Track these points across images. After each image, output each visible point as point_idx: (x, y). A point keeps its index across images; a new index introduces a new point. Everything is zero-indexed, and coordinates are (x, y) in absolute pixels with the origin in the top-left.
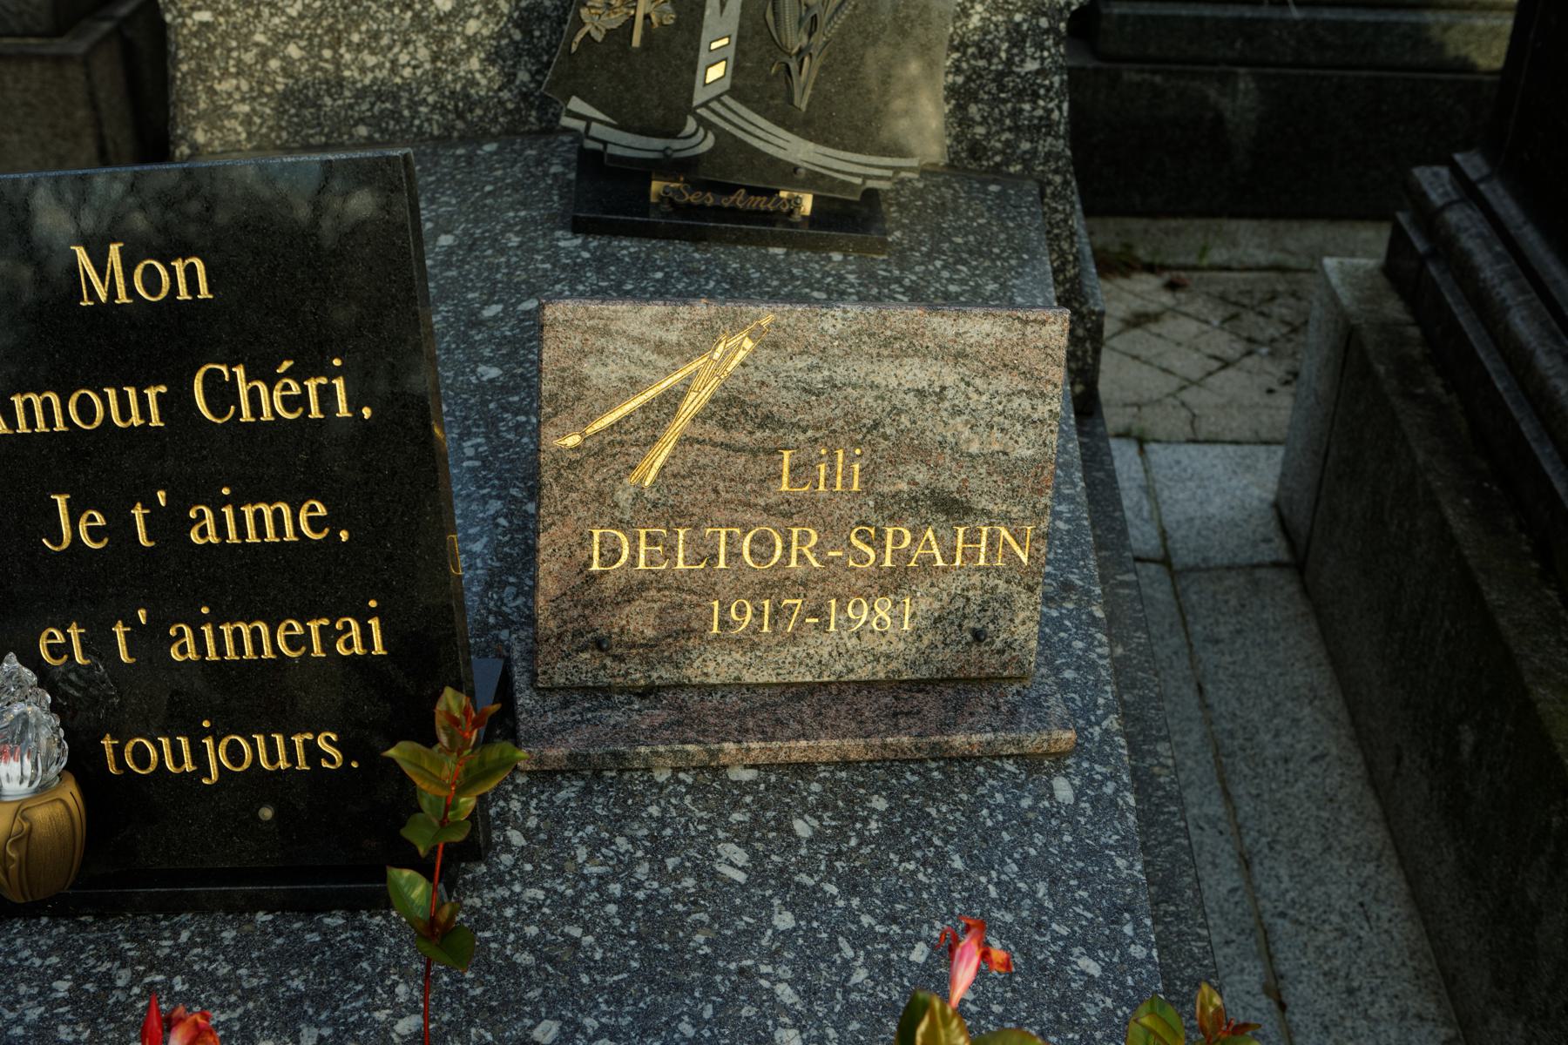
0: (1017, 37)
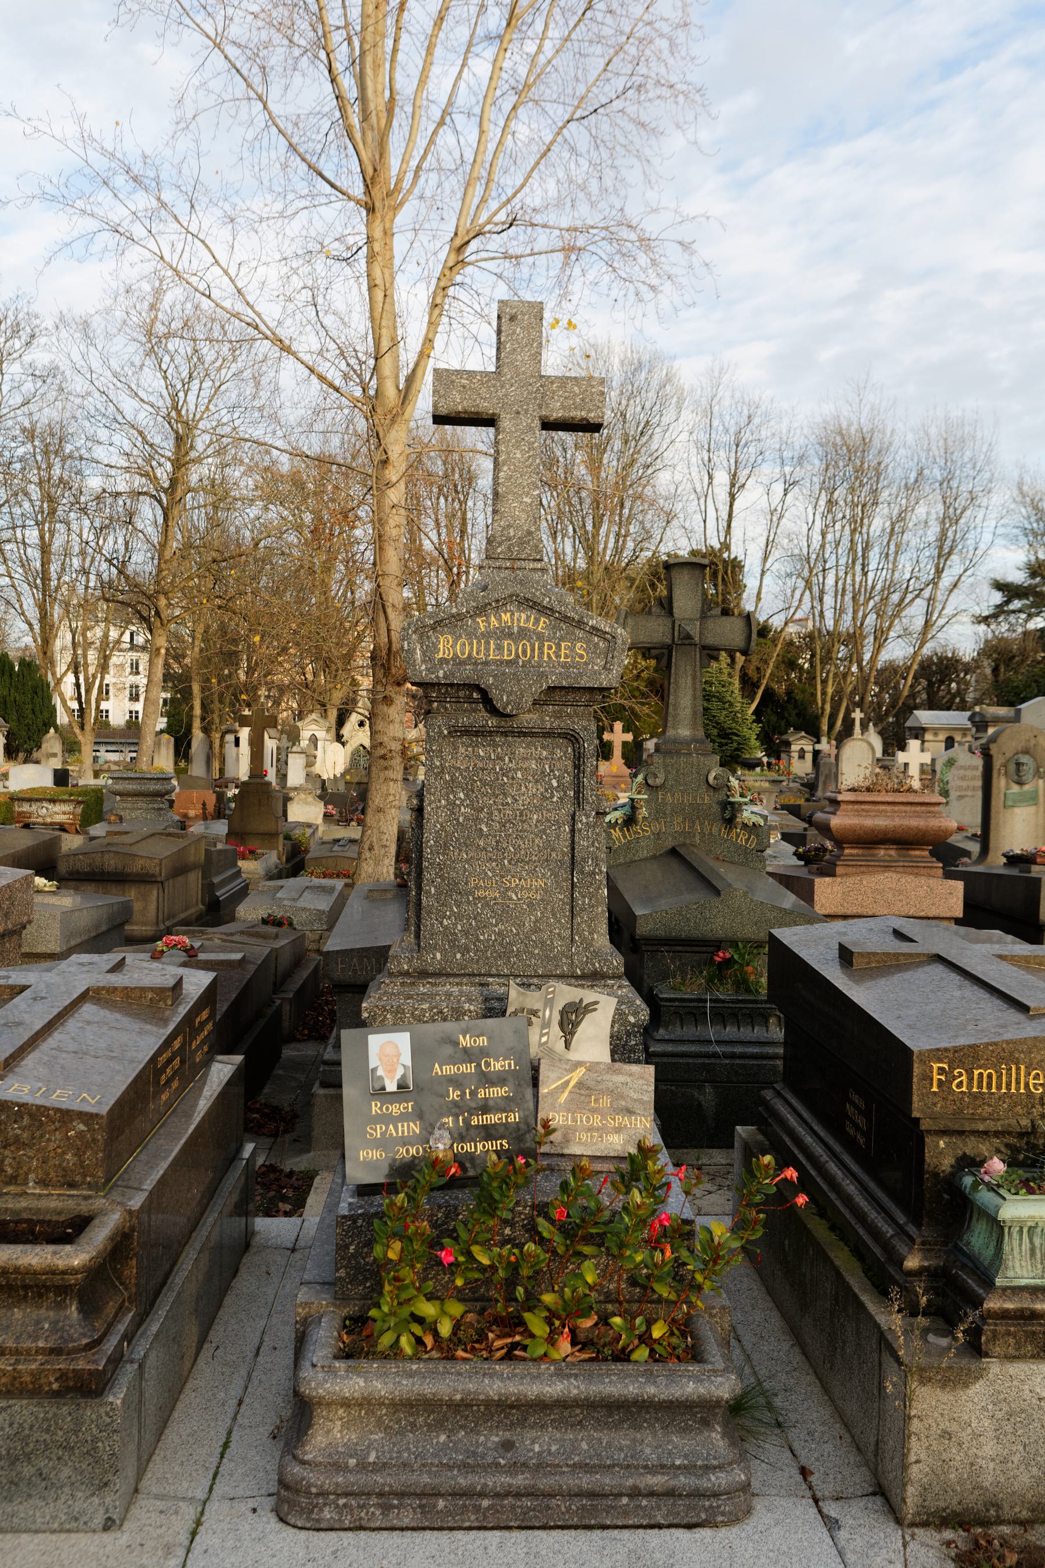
0: (628, 1034)
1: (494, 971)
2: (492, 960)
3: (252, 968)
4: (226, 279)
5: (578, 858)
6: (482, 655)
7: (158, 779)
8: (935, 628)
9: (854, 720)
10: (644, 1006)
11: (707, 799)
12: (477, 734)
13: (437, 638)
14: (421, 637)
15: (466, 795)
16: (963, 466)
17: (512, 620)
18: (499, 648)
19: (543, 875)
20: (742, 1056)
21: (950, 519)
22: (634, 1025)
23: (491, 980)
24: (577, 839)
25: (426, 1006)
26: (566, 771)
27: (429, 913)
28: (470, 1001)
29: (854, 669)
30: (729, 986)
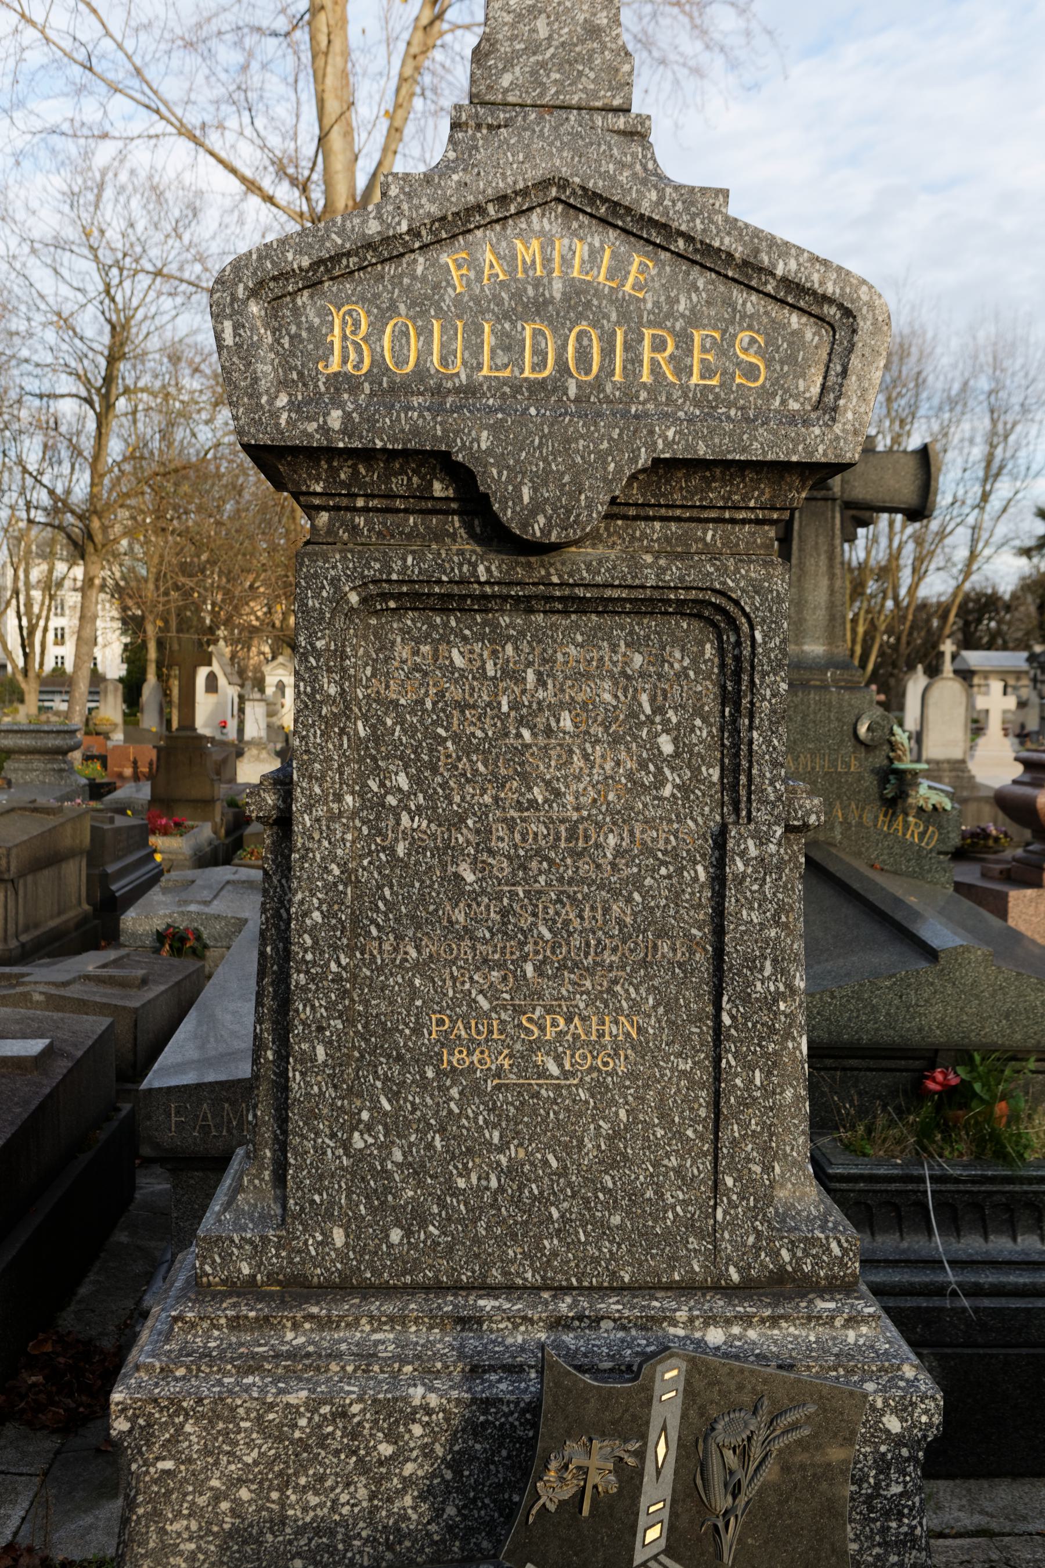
1: (496, 1275)
2: (490, 1246)
3: (61, 1067)
4: (120, 55)
5: (733, 955)
6: (458, 367)
7: (58, 732)
8: (980, 559)
9: (942, 654)
10: (926, 1384)
11: (856, 764)
12: (445, 604)
13: (324, 313)
14: (273, 313)
15: (417, 781)
16: (1013, 374)
17: (547, 261)
18: (509, 345)
19: (635, 1005)
20: (998, 1291)
21: (996, 437)
22: (898, 1441)
23: (487, 1304)
24: (730, 905)
25: (298, 1397)
26: (698, 712)
27: (311, 1116)
28: (427, 1375)
29: (890, 604)
30: (962, 1147)
